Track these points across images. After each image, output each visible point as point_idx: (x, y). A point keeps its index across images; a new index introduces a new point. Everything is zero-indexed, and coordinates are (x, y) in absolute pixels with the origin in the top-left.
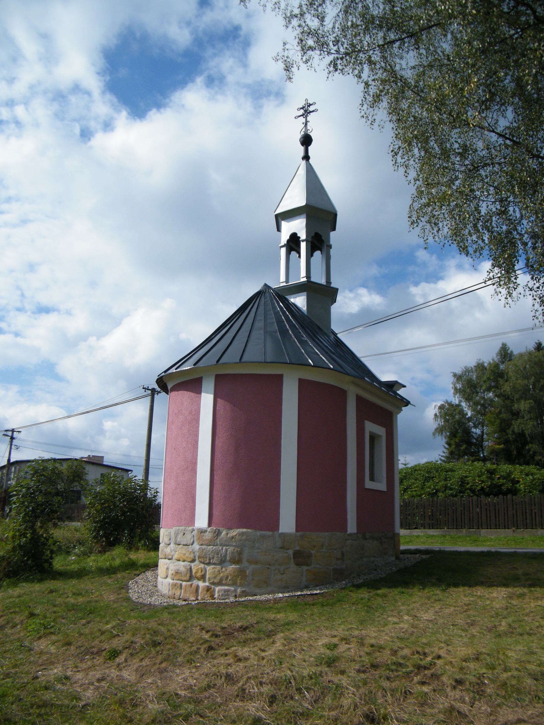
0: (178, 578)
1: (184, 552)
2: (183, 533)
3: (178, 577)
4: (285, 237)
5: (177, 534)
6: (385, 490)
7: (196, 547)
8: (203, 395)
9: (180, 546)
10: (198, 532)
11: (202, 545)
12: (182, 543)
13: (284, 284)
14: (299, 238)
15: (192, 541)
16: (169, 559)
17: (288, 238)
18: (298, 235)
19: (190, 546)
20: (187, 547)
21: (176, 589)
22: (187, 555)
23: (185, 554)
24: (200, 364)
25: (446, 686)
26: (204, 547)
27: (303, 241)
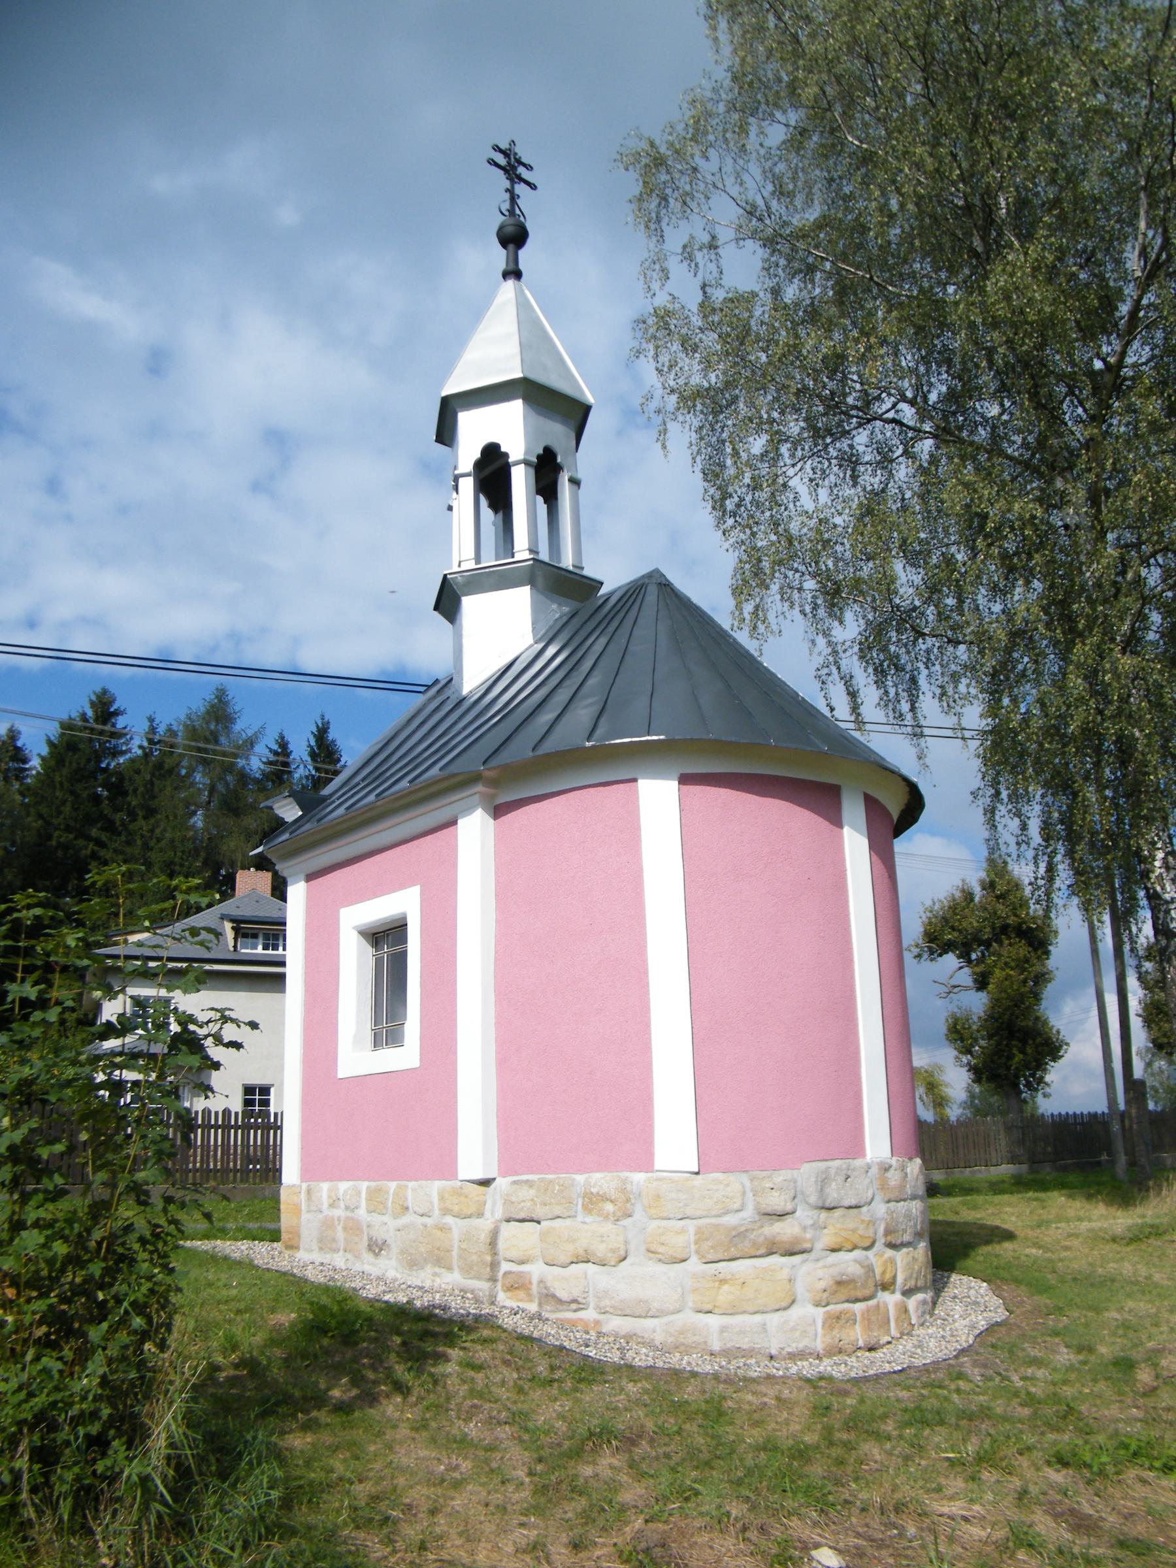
0: (844, 1298)
1: (851, 1225)
2: (843, 1178)
3: (844, 1293)
4: (468, 453)
5: (823, 1181)
6: (341, 1074)
7: (880, 1209)
8: (847, 831)
9: (837, 1213)
10: (880, 1169)
11: (888, 1202)
12: (847, 1203)
13: (471, 565)
14: (506, 455)
15: (870, 1195)
16: (867, 1249)
17: (478, 455)
18: (503, 449)
19: (865, 1209)
20: (855, 1210)
21: (842, 1327)
22: (860, 1232)
23: (854, 1231)
24: (453, 769)
25: (1041, 1497)
26: (892, 1204)
27: (517, 463)
